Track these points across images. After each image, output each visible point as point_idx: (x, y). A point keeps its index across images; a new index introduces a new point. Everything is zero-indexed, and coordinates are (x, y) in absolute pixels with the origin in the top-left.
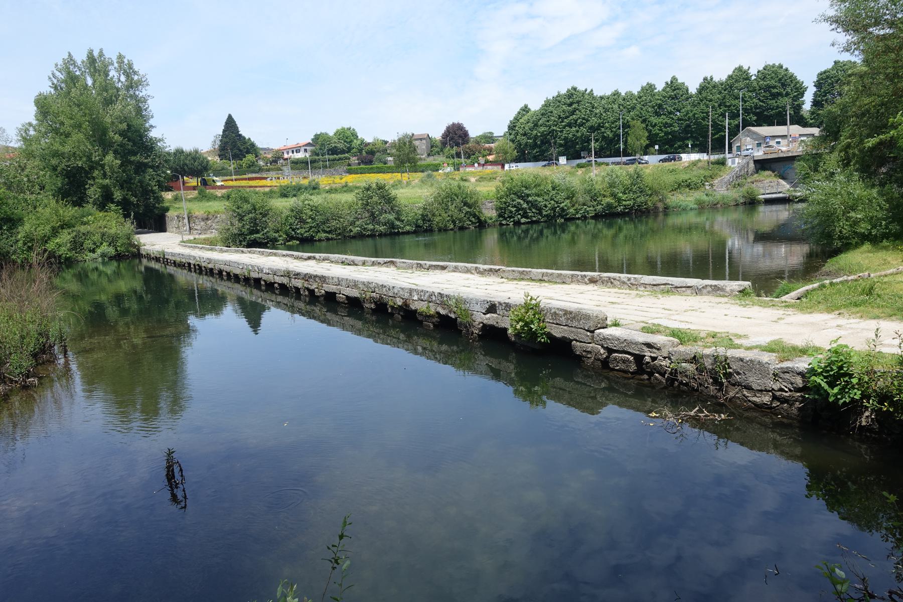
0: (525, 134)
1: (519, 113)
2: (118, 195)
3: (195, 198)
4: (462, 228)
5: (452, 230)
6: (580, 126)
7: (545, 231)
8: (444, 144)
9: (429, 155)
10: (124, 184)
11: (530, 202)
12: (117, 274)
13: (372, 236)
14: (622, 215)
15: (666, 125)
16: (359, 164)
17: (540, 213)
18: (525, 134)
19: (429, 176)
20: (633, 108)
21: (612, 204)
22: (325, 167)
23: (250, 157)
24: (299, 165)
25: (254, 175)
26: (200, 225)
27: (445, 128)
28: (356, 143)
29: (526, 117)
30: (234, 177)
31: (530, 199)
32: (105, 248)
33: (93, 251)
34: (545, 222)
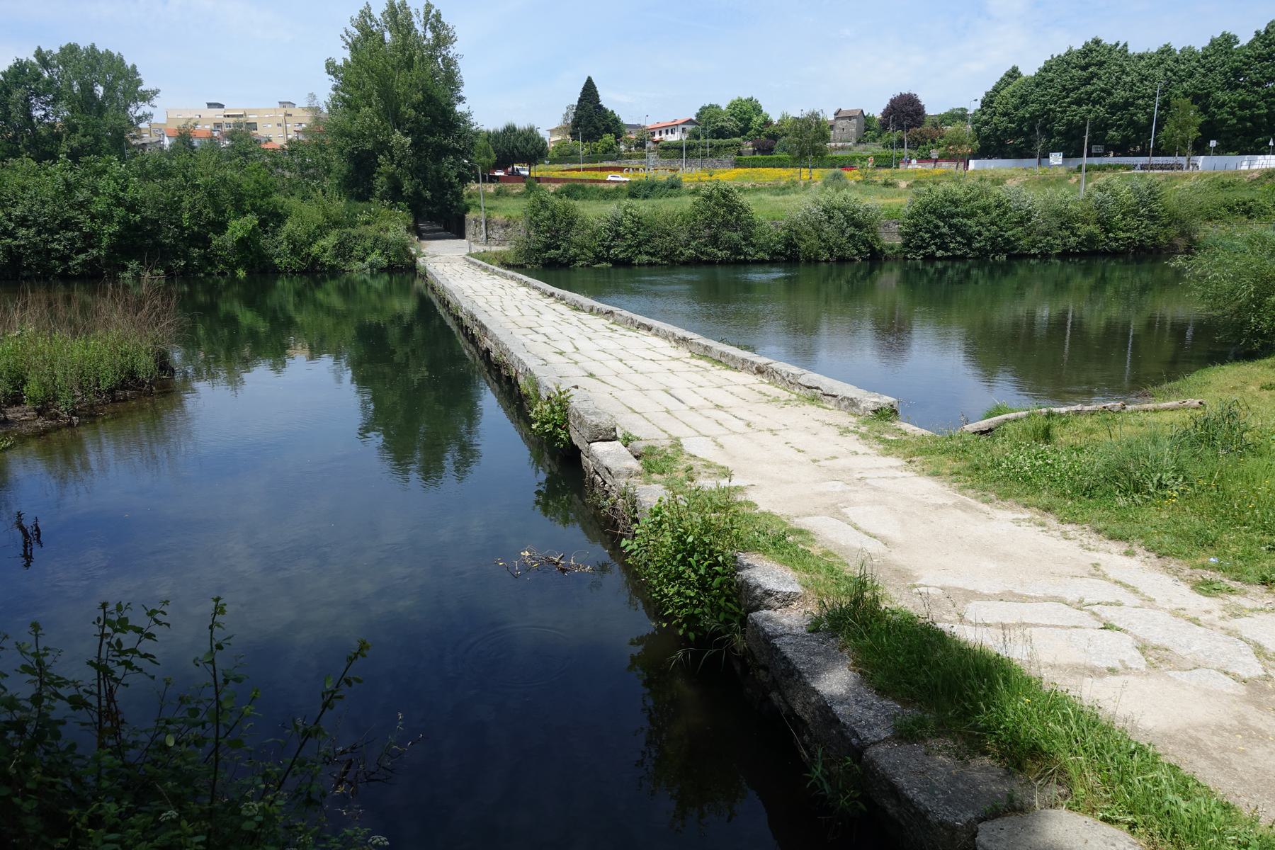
0: (1005, 114)
1: (1002, 79)
2: (407, 187)
3: (521, 194)
4: (842, 260)
5: (827, 261)
6: (1094, 103)
7: (974, 272)
8: (884, 125)
9: (859, 142)
10: (418, 171)
11: (955, 225)
12: (389, 289)
13: (710, 263)
14: (1114, 254)
15: (1243, 105)
16: (754, 153)
17: (969, 245)
18: (1005, 114)
19: (837, 177)
20: (1191, 75)
21: (1093, 233)
22: (704, 155)
23: (609, 138)
24: (671, 151)
25: (610, 164)
26: (498, 234)
27: (888, 102)
28: (757, 120)
29: (1011, 88)
30: (582, 166)
31: (955, 221)
32: (374, 257)
33: (363, 260)
34: (976, 258)
